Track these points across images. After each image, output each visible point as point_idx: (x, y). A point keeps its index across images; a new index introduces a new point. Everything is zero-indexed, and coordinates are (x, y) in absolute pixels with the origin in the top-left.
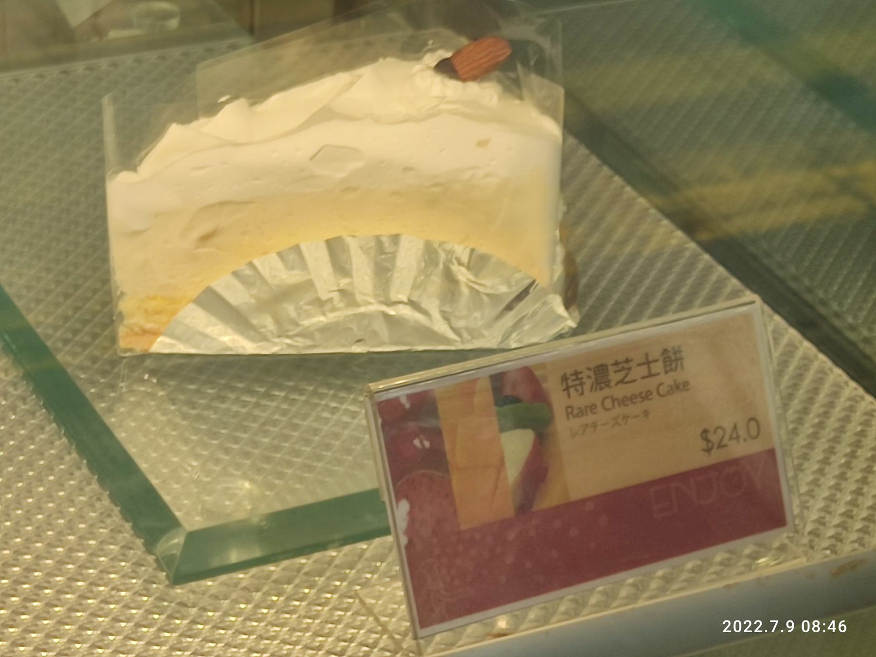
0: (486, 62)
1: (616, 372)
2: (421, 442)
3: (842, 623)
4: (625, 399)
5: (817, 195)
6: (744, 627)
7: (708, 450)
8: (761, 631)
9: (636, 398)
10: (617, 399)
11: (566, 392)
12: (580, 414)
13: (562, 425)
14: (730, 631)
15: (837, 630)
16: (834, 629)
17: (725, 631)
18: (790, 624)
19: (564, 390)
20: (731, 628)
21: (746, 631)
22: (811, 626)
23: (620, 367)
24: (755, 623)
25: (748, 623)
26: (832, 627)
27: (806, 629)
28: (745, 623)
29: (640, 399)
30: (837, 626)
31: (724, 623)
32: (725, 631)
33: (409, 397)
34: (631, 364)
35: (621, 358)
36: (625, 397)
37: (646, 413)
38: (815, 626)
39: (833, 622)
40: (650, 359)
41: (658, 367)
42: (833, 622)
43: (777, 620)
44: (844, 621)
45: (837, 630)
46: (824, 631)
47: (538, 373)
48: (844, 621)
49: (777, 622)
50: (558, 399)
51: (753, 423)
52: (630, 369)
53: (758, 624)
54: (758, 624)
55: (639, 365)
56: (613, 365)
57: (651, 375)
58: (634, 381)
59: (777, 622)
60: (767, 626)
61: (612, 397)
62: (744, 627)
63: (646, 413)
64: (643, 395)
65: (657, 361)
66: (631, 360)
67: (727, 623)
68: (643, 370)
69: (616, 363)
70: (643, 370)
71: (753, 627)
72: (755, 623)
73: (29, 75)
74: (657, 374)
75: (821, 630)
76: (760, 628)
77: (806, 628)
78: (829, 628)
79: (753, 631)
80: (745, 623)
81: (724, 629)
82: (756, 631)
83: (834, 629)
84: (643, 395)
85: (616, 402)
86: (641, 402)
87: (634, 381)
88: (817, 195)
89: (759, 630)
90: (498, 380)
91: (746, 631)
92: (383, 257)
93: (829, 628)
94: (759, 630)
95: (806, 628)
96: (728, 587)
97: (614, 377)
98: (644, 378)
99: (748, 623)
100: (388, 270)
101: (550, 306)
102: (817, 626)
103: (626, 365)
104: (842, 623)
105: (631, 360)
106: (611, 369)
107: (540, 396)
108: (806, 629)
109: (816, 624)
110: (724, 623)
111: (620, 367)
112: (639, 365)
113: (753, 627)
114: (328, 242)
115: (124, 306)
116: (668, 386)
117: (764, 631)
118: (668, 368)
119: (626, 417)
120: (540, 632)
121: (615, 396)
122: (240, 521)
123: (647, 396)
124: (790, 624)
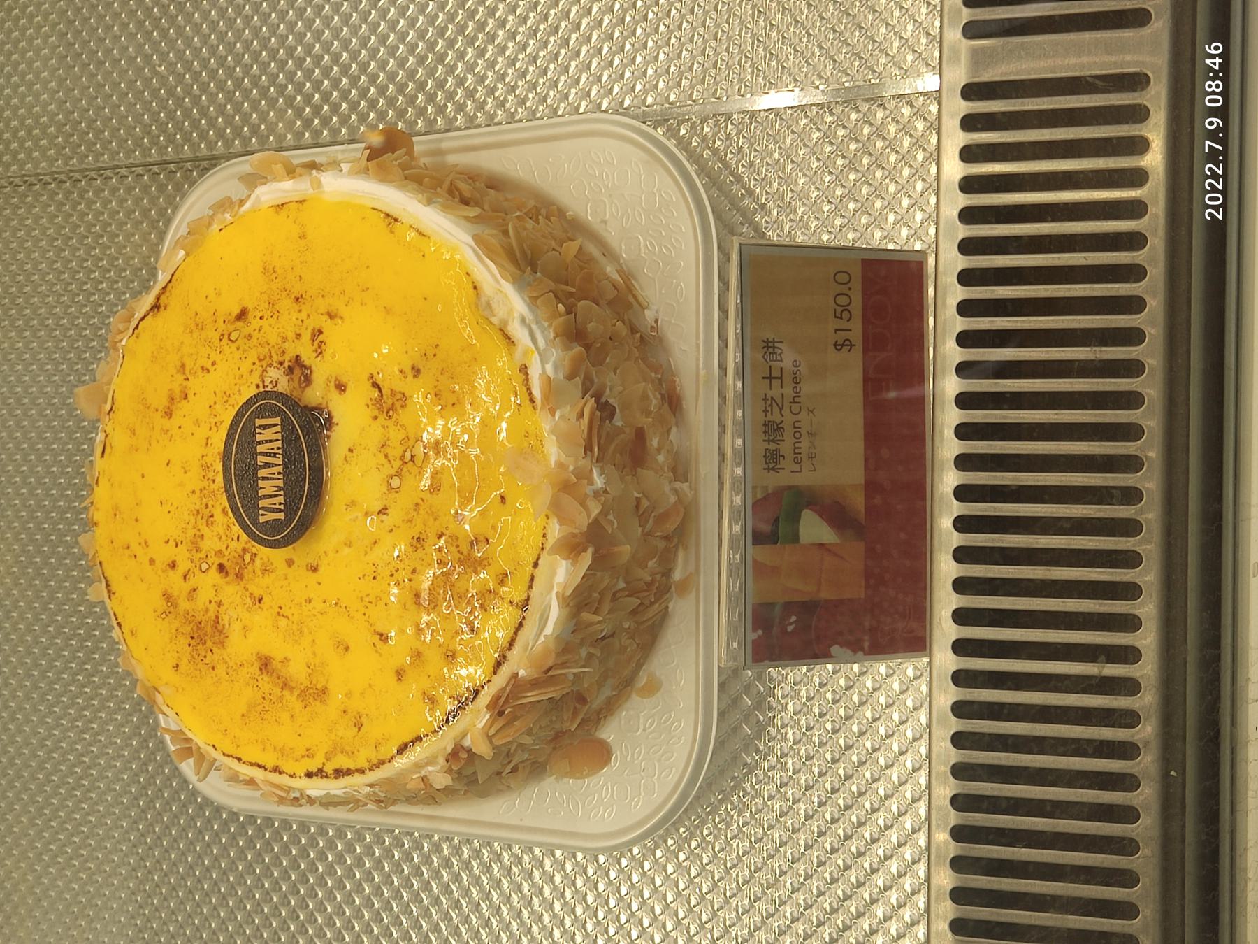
2: (791, 624)
6: (1214, 190)
13: (804, 478)
15: (1219, 56)
16: (1218, 61)
17: (1220, 217)
18: (1211, 123)
20: (1216, 208)
21: (1220, 187)
22: (1214, 93)
23: (769, 409)
24: (1209, 173)
25: (1210, 184)
26: (1215, 64)
27: (1217, 101)
30: (1213, 57)
31: (1209, 218)
32: (1220, 217)
33: (754, 630)
34: (768, 397)
38: (1214, 88)
39: (1208, 61)
42: (1208, 61)
45: (1219, 56)
46: (1221, 75)
47: (759, 496)
49: (1207, 142)
50: (785, 478)
52: (772, 398)
53: (1210, 169)
54: (1210, 169)
62: (1214, 190)
67: (1210, 214)
69: (765, 411)
71: (1215, 176)
75: (1219, 79)
77: (1217, 101)
78: (1217, 68)
79: (1221, 176)
80: (1209, 188)
82: (1220, 172)
83: (1218, 61)
90: (759, 538)
91: (1220, 187)
93: (1217, 68)
95: (1217, 101)
97: (776, 417)
99: (1210, 184)
102: (1214, 84)
103: (769, 402)
106: (770, 418)
107: (778, 494)
108: (1217, 101)
109: (1210, 86)
110: (1209, 218)
111: (769, 409)
113: (1215, 176)
117: (1221, 161)
118: (779, 358)
124: (1211, 123)
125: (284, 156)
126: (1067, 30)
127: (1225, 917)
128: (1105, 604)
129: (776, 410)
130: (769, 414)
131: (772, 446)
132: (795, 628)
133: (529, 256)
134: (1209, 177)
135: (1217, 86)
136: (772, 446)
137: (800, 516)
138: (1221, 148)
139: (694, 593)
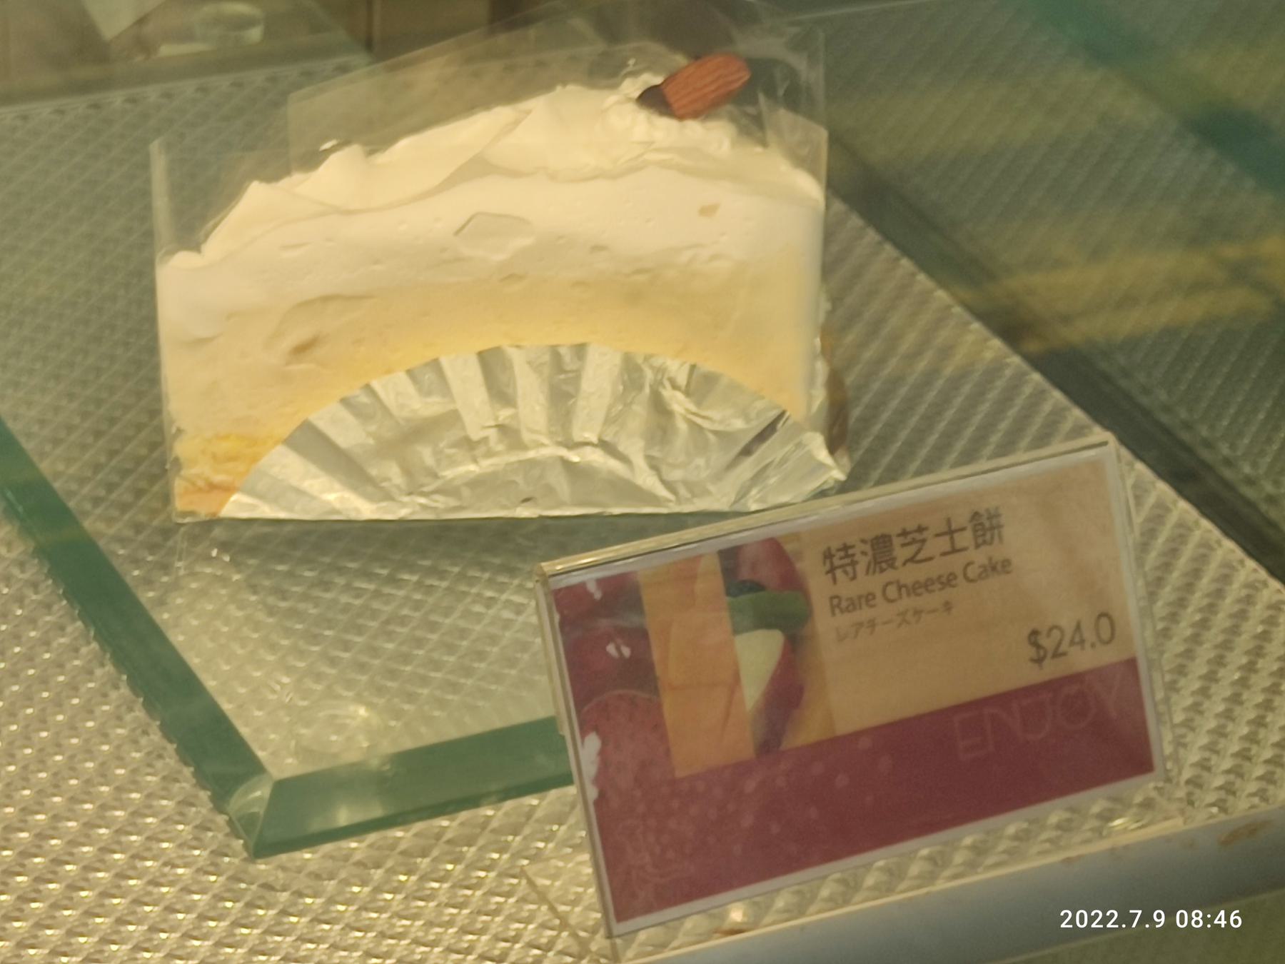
0: (713, 91)
1: (904, 545)
3: (1236, 915)
4: (917, 586)
5: (1199, 286)
6: (1091, 920)
7: (1039, 661)
8: (1117, 926)
9: (933, 584)
10: (905, 586)
11: (830, 575)
12: (851, 608)
14: (1071, 926)
15: (1228, 924)
16: (1223, 923)
17: (1063, 926)
18: (1159, 916)
19: (828, 572)
20: (1072, 921)
21: (1094, 926)
22: (1190, 919)
23: (909, 538)
24: (1108, 914)
25: (1097, 915)
26: (1220, 920)
27: (1182, 923)
28: (1093, 914)
29: (940, 586)
30: (1227, 918)
31: (1062, 914)
32: (1063, 926)
33: (600, 582)
34: (925, 534)
35: (911, 526)
36: (917, 582)
37: (948, 606)
38: (1195, 919)
39: (1222, 913)
40: (954, 526)
41: (965, 539)
42: (1222, 913)
43: (1140, 910)
44: (1238, 911)
45: (1228, 924)
46: (1209, 926)
47: (789, 548)
48: (1238, 911)
49: (1140, 912)
50: (818, 585)
51: (1104, 621)
52: (924, 541)
53: (1112, 915)
54: (1112, 915)
55: (938, 535)
56: (899, 535)
57: (954, 550)
58: (930, 559)
59: (1140, 912)
60: (1126, 918)
61: (898, 582)
62: (1091, 920)
63: (948, 606)
64: (944, 579)
65: (963, 529)
66: (926, 529)
67: (1066, 915)
68: (944, 544)
69: (904, 533)
70: (944, 544)
71: (1105, 920)
72: (1108, 914)
73: (43, 110)
74: (964, 549)
75: (1205, 924)
76: (1115, 921)
77: (1182, 922)
78: (1216, 922)
79: (1105, 926)
80: (1093, 914)
81: (1062, 923)
82: (1109, 926)
83: (1223, 923)
84: (944, 579)
85: (904, 590)
86: (941, 589)
87: (930, 559)
88: (1199, 286)
89: (1113, 924)
90: (730, 557)
91: (1094, 926)
92: (562, 377)
93: (1216, 922)
94: (1113, 924)
95: (1182, 922)
96: (1068, 861)
97: (901, 553)
98: (944, 554)
99: (1097, 915)
100: (569, 396)
101: (807, 449)
102: (1199, 919)
103: (918, 536)
104: (1236, 915)
105: (926, 529)
106: (897, 542)
107: (792, 581)
108: (1182, 923)
109: (1197, 915)
110: (1062, 914)
111: (909, 538)
112: (938, 535)
113: (1105, 920)
114: (481, 355)
115: (182, 449)
116: (980, 567)
117: (1120, 926)
118: (980, 540)
119: (918, 613)
120: (792, 927)
121: (903, 582)
122: (353, 765)
123: (949, 581)
124: (1159, 916)
132: (628, 645)
133: (650, 948)
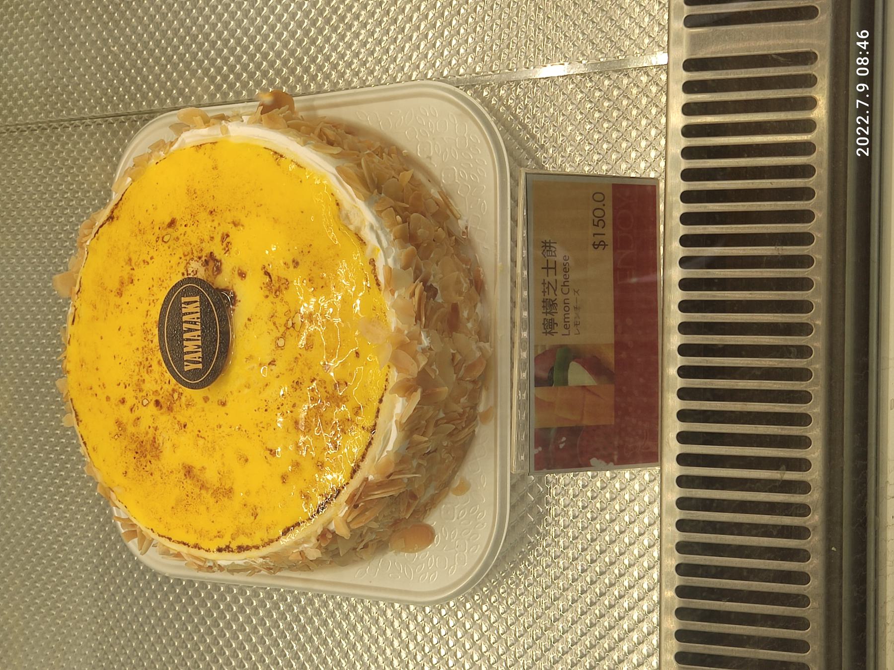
2: (562, 443)
6: (863, 135)
13: (572, 339)
15: (867, 40)
16: (865, 43)
17: (867, 154)
18: (861, 88)
20: (864, 148)
21: (867, 133)
22: (862, 66)
23: (546, 290)
24: (859, 123)
25: (860, 131)
26: (863, 45)
27: (865, 72)
30: (862, 40)
31: (859, 155)
32: (867, 154)
33: (536, 447)
34: (546, 281)
38: (862, 62)
39: (859, 44)
42: (859, 44)
45: (867, 40)
46: (868, 53)
47: (539, 352)
49: (858, 101)
50: (558, 339)
52: (549, 283)
53: (860, 120)
54: (860, 120)
62: (863, 135)
67: (860, 152)
69: (544, 292)
71: (863, 125)
75: (867, 56)
77: (865, 72)
78: (865, 48)
79: (867, 125)
80: (859, 134)
82: (867, 122)
83: (865, 43)
90: (539, 382)
91: (867, 133)
93: (865, 48)
95: (865, 72)
97: (551, 296)
99: (860, 131)
102: (862, 60)
103: (546, 286)
106: (547, 296)
107: (553, 351)
108: (865, 72)
109: (860, 61)
110: (859, 155)
111: (546, 290)
113: (863, 125)
117: (868, 115)
118: (553, 254)
124: (861, 88)
125: (202, 111)
126: (759, 21)
127: (870, 651)
128: (786, 429)
129: (551, 291)
130: (546, 294)
131: (549, 317)
134: (859, 126)
135: (865, 61)
136: (549, 317)
137: (568, 366)
138: (867, 105)
139: (493, 421)
